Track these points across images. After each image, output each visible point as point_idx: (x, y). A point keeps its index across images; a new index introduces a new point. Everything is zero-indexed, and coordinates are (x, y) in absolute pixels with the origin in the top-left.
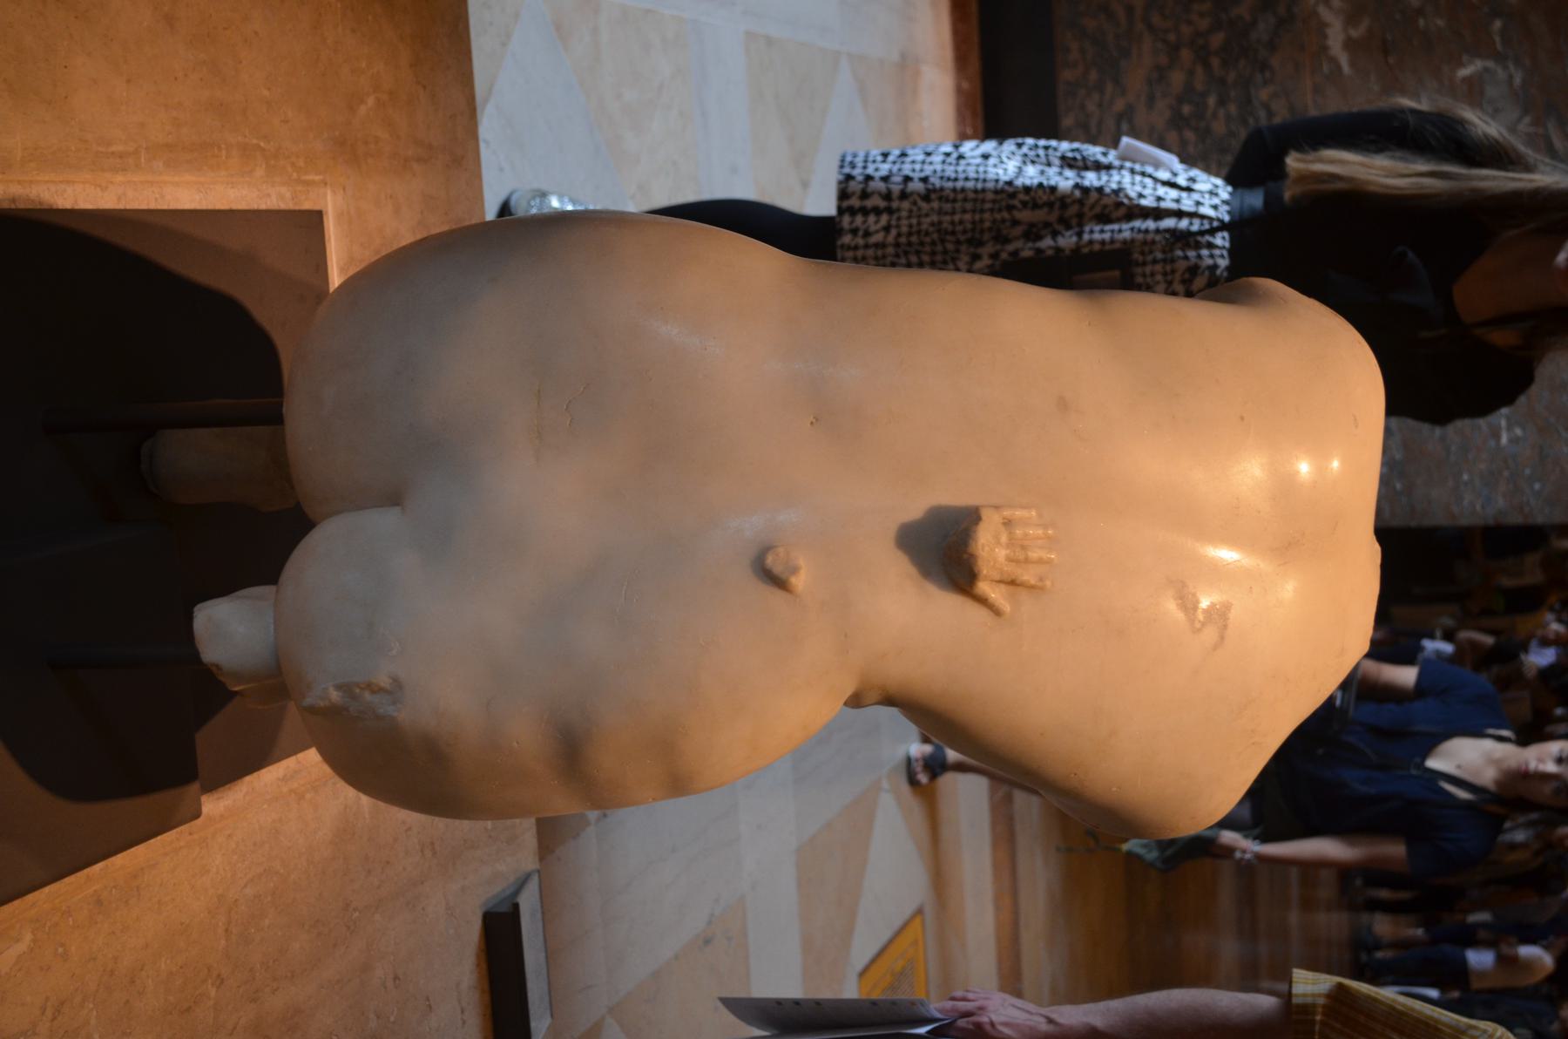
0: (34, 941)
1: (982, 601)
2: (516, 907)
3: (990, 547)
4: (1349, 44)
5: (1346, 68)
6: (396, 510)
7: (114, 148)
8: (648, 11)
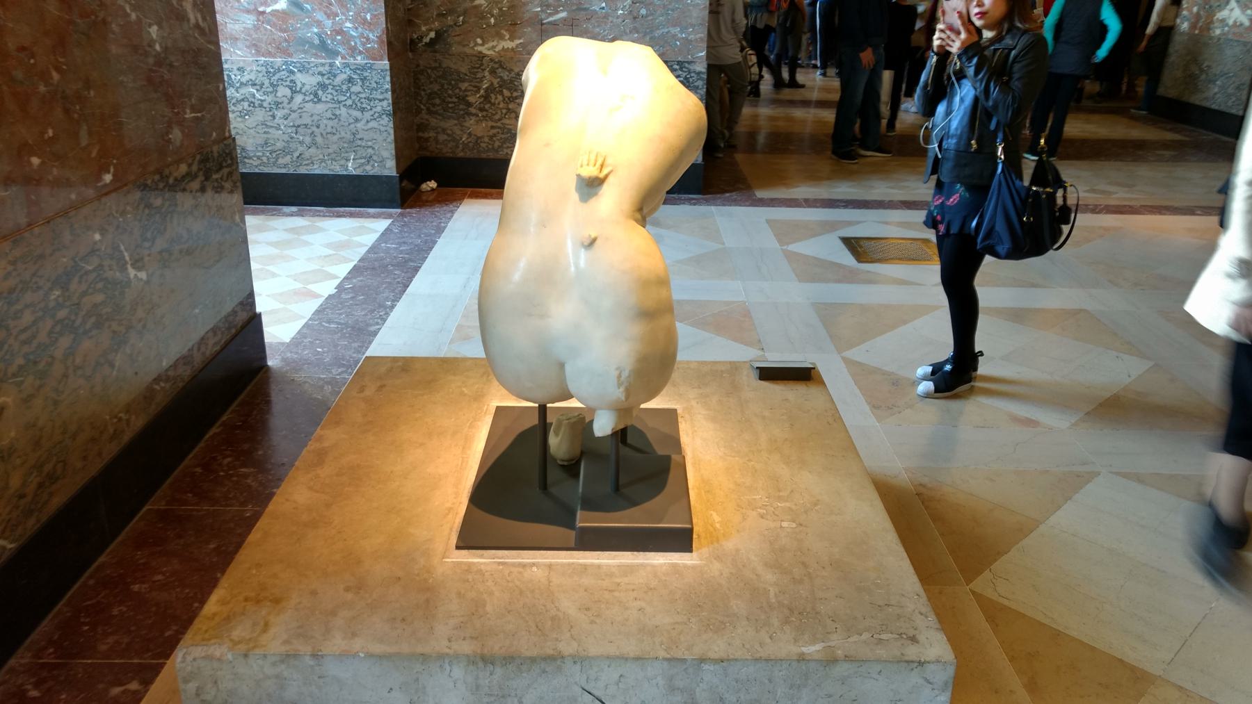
0: (714, 510)
1: (606, 176)
2: (757, 368)
3: (590, 171)
4: (512, 39)
5: (521, 41)
6: (566, 365)
7: (460, 464)
8: (465, 308)
